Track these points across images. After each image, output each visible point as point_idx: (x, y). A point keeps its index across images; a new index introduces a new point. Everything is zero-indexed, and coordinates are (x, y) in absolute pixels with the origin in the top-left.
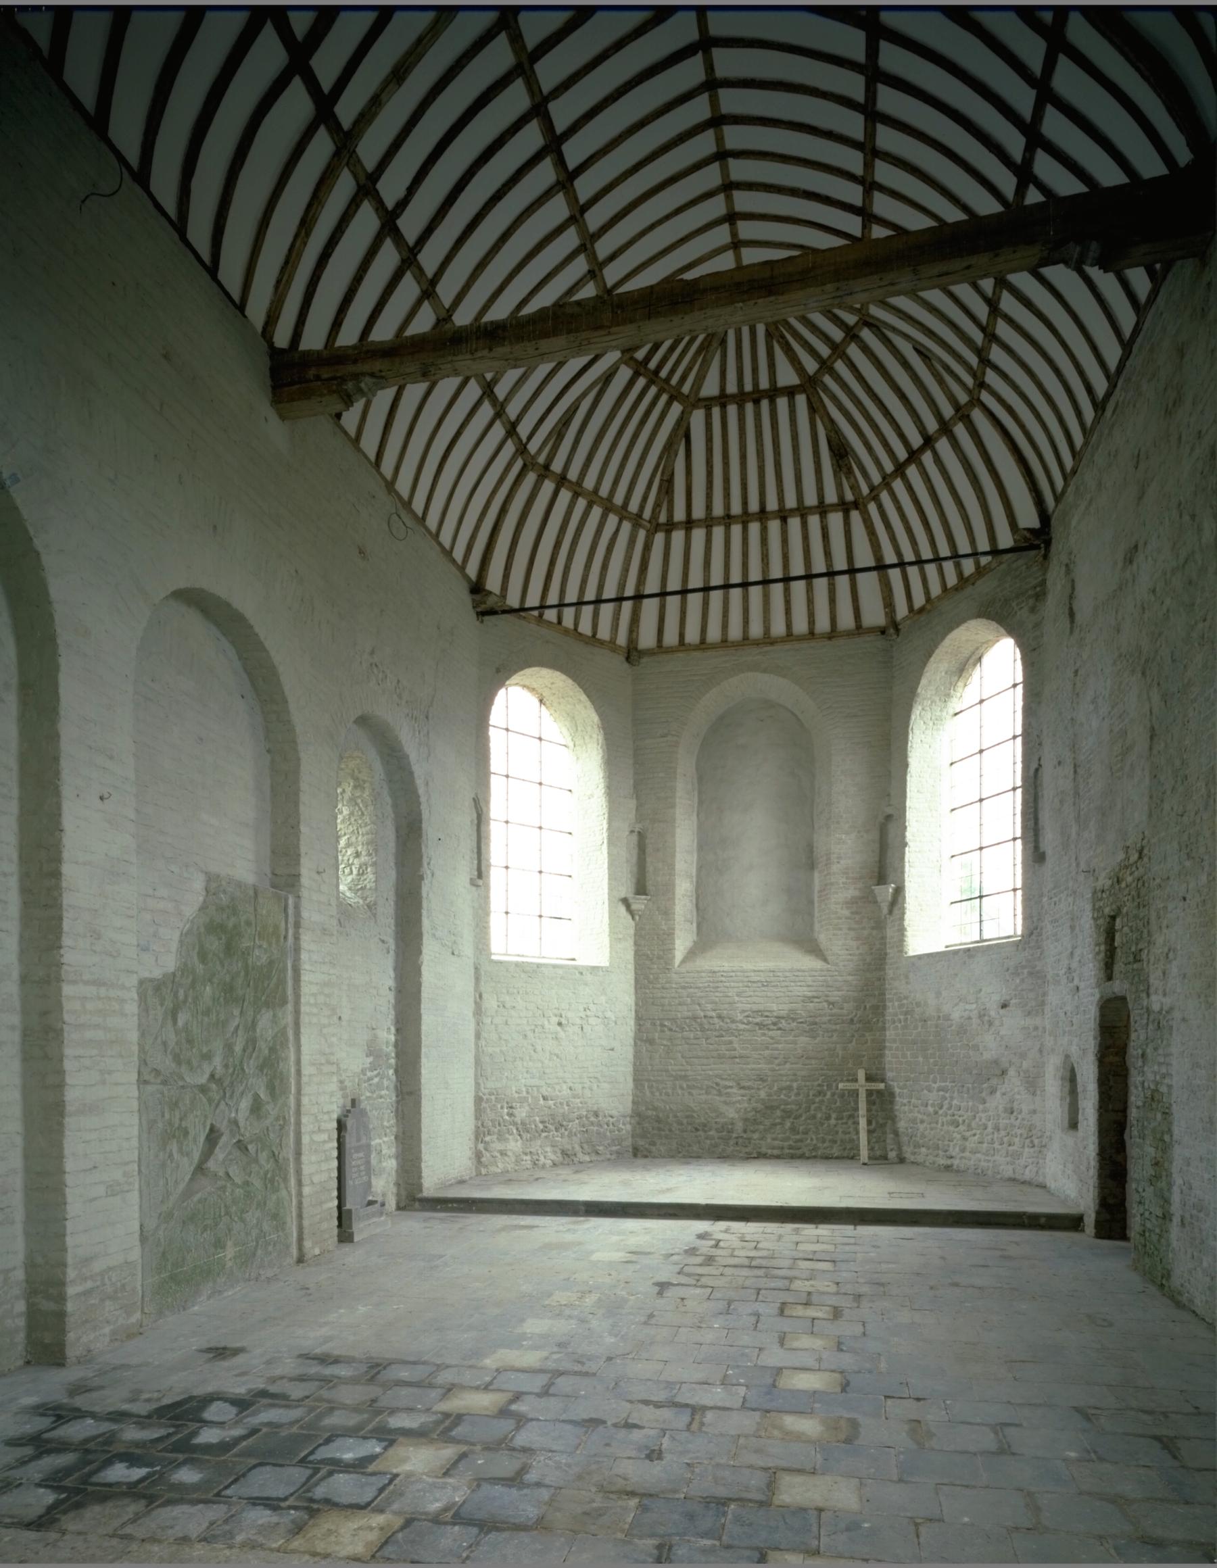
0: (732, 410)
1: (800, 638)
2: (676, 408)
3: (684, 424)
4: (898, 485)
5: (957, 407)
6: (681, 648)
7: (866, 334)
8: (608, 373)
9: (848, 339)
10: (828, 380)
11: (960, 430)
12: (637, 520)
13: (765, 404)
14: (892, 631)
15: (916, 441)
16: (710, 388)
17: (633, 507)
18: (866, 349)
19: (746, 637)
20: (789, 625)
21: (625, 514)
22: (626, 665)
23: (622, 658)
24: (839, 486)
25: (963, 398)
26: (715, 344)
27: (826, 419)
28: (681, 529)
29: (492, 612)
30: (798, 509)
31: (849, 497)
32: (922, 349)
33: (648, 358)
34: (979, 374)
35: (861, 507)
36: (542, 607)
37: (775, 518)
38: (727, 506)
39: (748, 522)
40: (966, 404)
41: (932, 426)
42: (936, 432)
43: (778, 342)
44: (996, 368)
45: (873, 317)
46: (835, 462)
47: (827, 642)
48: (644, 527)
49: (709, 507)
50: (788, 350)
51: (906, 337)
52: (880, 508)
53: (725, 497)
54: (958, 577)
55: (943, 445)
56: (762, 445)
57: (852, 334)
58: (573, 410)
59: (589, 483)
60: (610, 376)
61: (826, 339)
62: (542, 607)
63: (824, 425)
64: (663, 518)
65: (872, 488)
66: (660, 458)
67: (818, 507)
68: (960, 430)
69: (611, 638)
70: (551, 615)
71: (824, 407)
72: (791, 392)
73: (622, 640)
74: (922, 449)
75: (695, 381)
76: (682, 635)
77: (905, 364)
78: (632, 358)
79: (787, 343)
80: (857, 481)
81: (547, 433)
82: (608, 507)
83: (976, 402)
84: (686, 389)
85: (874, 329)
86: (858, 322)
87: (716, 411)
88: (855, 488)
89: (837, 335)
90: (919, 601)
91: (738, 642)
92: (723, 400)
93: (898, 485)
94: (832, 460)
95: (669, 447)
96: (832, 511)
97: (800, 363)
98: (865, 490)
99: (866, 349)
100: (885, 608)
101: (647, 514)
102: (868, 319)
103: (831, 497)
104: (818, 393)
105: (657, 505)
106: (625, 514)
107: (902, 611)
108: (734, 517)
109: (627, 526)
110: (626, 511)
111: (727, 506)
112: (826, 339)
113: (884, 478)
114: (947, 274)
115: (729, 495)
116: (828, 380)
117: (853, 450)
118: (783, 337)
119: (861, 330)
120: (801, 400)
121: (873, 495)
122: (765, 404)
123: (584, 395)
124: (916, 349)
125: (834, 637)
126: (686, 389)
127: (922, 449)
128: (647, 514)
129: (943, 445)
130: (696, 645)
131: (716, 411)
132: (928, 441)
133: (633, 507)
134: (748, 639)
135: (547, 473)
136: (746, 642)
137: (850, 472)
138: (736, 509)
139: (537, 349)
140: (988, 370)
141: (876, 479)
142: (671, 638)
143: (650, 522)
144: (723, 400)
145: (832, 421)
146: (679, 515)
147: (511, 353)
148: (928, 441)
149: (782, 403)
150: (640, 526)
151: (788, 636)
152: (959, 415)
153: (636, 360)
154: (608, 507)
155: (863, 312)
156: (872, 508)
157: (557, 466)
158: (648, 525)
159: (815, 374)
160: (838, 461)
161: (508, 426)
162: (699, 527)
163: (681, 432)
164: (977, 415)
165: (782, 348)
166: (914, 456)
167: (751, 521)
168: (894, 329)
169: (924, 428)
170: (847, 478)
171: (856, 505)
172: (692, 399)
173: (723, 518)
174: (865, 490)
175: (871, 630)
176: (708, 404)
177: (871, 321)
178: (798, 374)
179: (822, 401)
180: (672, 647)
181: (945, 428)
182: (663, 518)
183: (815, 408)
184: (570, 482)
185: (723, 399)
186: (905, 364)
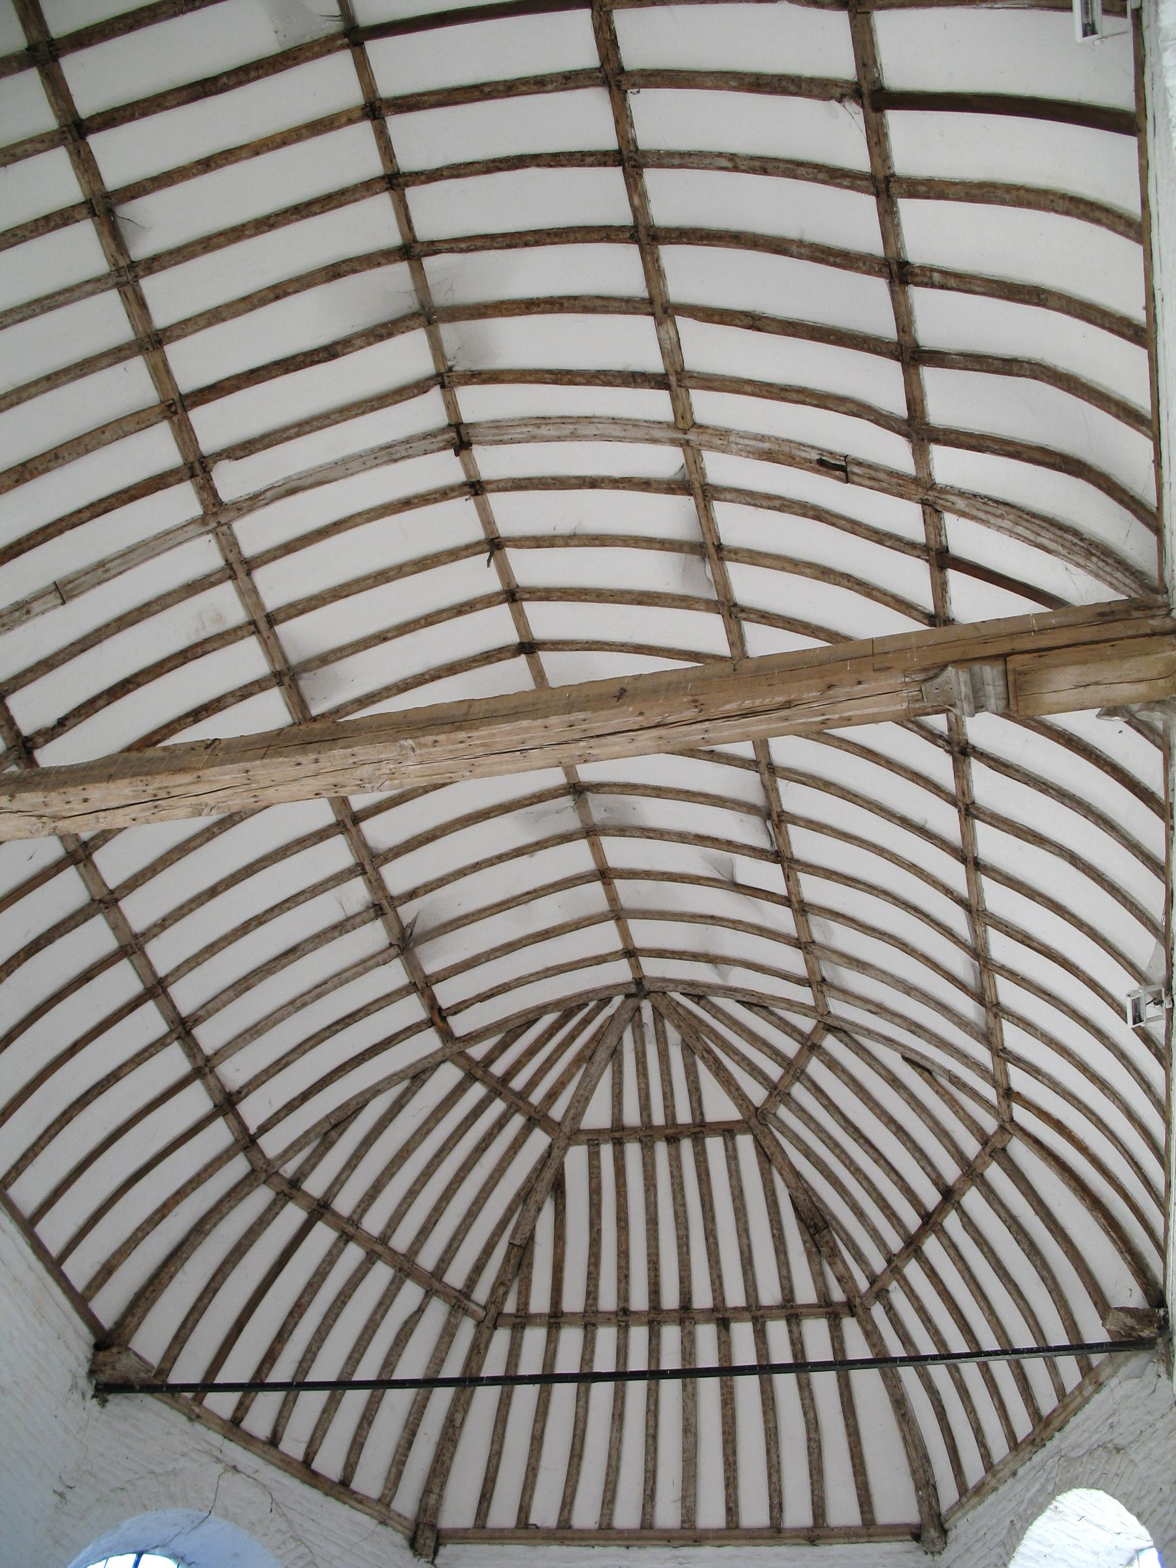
0: (633, 1151)
1: (754, 1536)
2: (539, 1141)
3: (553, 1164)
4: (913, 1270)
5: (984, 1140)
6: (520, 1533)
7: (831, 1043)
8: (420, 1067)
9: (806, 1052)
10: (783, 1112)
11: (995, 1173)
12: (460, 1301)
13: (686, 1146)
14: (933, 1533)
15: (931, 1197)
16: (598, 1115)
17: (456, 1276)
18: (833, 1065)
19: (647, 1523)
20: (732, 1510)
21: (436, 1285)
22: (409, 1554)
23: (400, 1539)
24: (818, 1277)
25: (990, 1124)
26: (602, 1054)
27: (786, 1171)
28: (541, 1325)
29: (124, 1387)
30: (747, 1309)
31: (838, 1295)
32: (917, 1059)
33: (490, 1058)
34: (998, 1076)
35: (859, 1310)
36: (208, 1385)
37: (707, 1321)
38: (623, 1294)
39: (659, 1323)
40: (995, 1133)
41: (951, 1172)
42: (958, 1180)
43: (702, 1058)
44: (1019, 1061)
45: (837, 1018)
46: (807, 1237)
47: (808, 1550)
48: (472, 1315)
49: (592, 1293)
50: (719, 1070)
51: (889, 1041)
52: (890, 1310)
53: (619, 1281)
54: (1032, 1420)
55: (973, 1200)
56: (684, 1205)
57: (811, 1046)
58: (352, 1108)
59: (373, 1223)
60: (424, 1072)
61: (775, 1054)
62: (208, 1385)
63: (784, 1180)
64: (510, 1307)
65: (873, 1279)
66: (510, 1211)
67: (781, 1307)
68: (995, 1173)
69: (383, 1496)
70: (222, 1404)
71: (783, 1151)
72: (728, 1131)
73: (406, 1502)
74: (941, 1209)
75: (571, 1103)
76: (524, 1510)
77: (895, 1082)
78: (462, 1054)
79: (717, 1060)
80: (847, 1269)
81: (300, 1132)
82: (405, 1267)
83: (1009, 1127)
84: (557, 1112)
85: (842, 1035)
86: (816, 1028)
87: (607, 1151)
88: (845, 1279)
89: (790, 1047)
90: (974, 1471)
91: (629, 1531)
92: (617, 1135)
93: (913, 1270)
94: (802, 1234)
95: (525, 1195)
96: (808, 1315)
97: (738, 1089)
98: (863, 1284)
99: (833, 1065)
100: (918, 1489)
101: (481, 1293)
102: (829, 1021)
103: (806, 1293)
104: (771, 1133)
105: (501, 1284)
106: (436, 1285)
107: (948, 1493)
108: (635, 1313)
109: (437, 1311)
110: (440, 1280)
111: (623, 1294)
112: (775, 1054)
113: (889, 1261)
114: (754, 713)
115: (627, 1276)
116: (783, 1112)
117: (835, 1218)
118: (710, 1051)
119: (823, 1038)
120: (745, 1143)
121: (875, 1289)
122: (686, 1146)
123: (375, 1091)
124: (905, 1059)
125: (819, 1537)
126: (557, 1112)
127: (941, 1209)
128: (481, 1293)
129: (973, 1200)
130: (548, 1530)
131: (607, 1151)
132: (949, 1195)
133: (456, 1276)
134: (651, 1527)
135: (294, 1192)
136: (645, 1533)
137: (834, 1254)
138: (639, 1301)
139: (86, 800)
140: (1011, 1068)
141: (878, 1263)
142: (503, 1515)
143: (485, 1308)
144: (617, 1135)
145: (798, 1175)
146: (540, 1302)
147: (46, 804)
148: (949, 1195)
149: (715, 1146)
150: (466, 1312)
151: (728, 1528)
152: (988, 1150)
153: (469, 1059)
154: (405, 1267)
155: (820, 1010)
156: (878, 1312)
157: (315, 1186)
158: (482, 1313)
159: (764, 1104)
160: (812, 1236)
161: (220, 1097)
162: (570, 1324)
163: (548, 1175)
164: (1018, 1149)
165: (709, 1067)
166: (930, 1221)
167: (665, 1322)
168: (869, 1033)
169: (939, 1176)
170: (830, 1264)
171: (850, 1308)
172: (566, 1129)
173: (616, 1313)
174: (863, 1284)
175: (893, 1532)
176: (594, 1139)
177: (836, 1023)
178: (736, 1104)
179: (778, 1144)
180: (501, 1530)
181: (972, 1173)
182: (510, 1307)
183: (767, 1157)
184: (335, 1214)
185: (618, 1134)
186: (895, 1082)
